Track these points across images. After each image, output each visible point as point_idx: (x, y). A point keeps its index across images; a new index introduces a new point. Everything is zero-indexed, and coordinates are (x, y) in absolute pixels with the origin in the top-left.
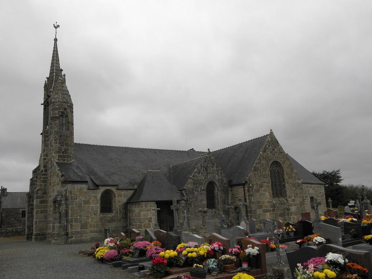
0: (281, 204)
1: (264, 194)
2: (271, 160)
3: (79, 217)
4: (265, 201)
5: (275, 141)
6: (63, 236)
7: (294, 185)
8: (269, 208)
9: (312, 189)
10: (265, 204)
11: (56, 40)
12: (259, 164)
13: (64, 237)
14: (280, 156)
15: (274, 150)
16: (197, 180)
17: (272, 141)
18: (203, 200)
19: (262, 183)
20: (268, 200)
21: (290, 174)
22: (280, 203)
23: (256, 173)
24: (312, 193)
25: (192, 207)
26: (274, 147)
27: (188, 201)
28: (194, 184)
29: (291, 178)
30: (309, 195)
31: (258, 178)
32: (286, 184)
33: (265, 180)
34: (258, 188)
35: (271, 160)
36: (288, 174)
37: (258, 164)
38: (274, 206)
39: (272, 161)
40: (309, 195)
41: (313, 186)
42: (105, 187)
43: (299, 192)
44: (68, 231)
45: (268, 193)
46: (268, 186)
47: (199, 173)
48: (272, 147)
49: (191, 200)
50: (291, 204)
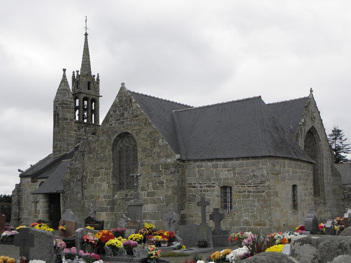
0: (125, 201)
1: (100, 186)
2: (116, 132)
3: (27, 206)
4: (100, 195)
5: (125, 100)
6: (13, 221)
7: (155, 168)
8: (106, 206)
9: (228, 171)
10: (100, 200)
11: (86, 35)
12: (97, 143)
13: (14, 221)
14: (132, 123)
15: (122, 115)
16: (74, 168)
17: (121, 101)
18: (79, 192)
19: (98, 169)
20: (105, 194)
21: (148, 149)
22: (124, 198)
23: (91, 156)
24: (227, 179)
25: (68, 200)
26: (124, 110)
27: (64, 194)
28: (71, 174)
29: (151, 156)
30: (217, 183)
31: (94, 162)
32: (140, 167)
33: (103, 164)
34: (93, 177)
35: (116, 132)
36: (144, 150)
37: (95, 142)
38: (113, 203)
39: (116, 135)
40: (217, 183)
41: (230, 163)
42: (41, 180)
43: (167, 180)
44: (20, 217)
45: (107, 183)
46: (107, 174)
47: (76, 161)
48: (119, 112)
49: (67, 193)
50: (145, 200)
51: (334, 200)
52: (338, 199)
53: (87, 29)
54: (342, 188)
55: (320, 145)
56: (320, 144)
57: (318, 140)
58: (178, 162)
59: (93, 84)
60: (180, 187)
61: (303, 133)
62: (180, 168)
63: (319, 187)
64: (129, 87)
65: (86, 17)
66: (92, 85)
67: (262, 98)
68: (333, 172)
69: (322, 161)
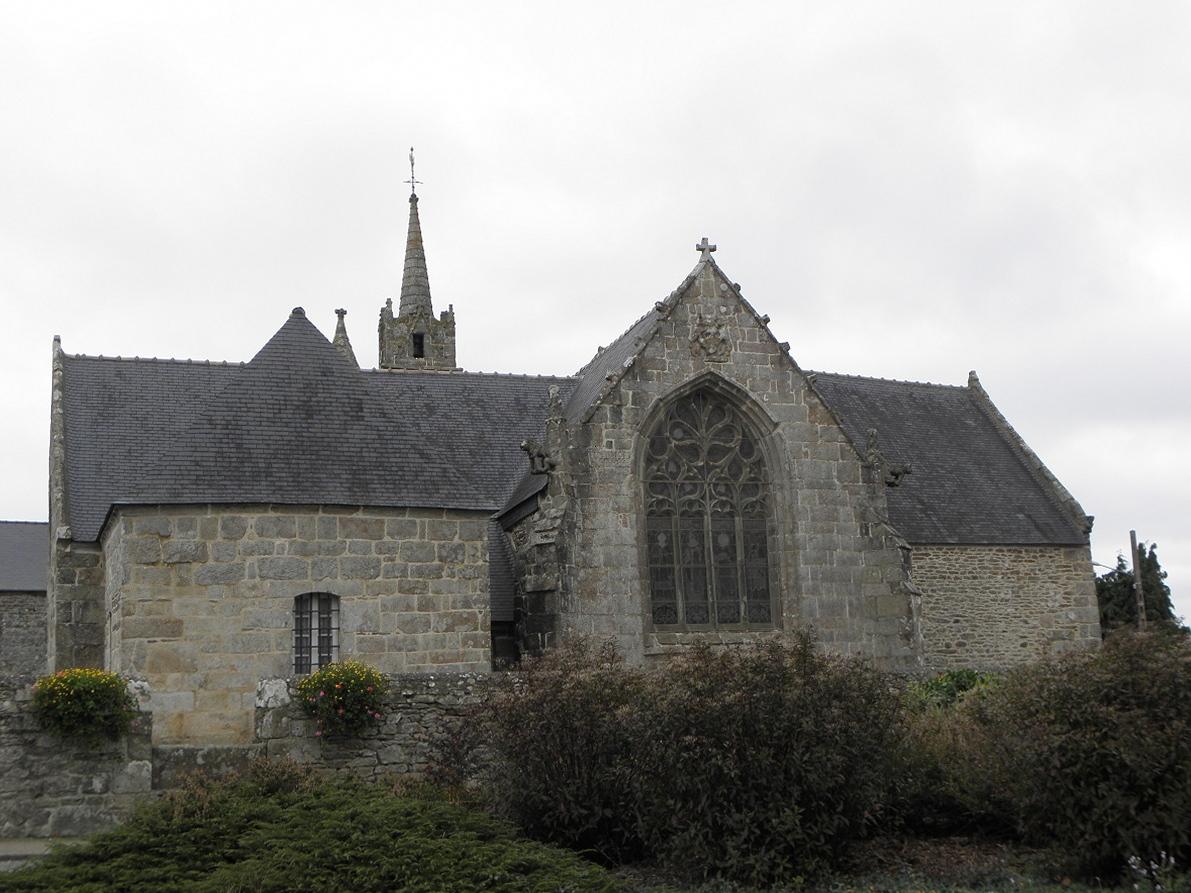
11: (414, 199)
51: (870, 640)
52: (886, 636)
53: (416, 185)
54: (901, 591)
55: (777, 439)
56: (779, 435)
57: (761, 420)
58: (68, 550)
59: (433, 338)
60: (73, 623)
61: (629, 405)
62: (79, 566)
63: (781, 596)
64: (70, 349)
65: (412, 150)
66: (428, 341)
67: (306, 316)
68: (867, 533)
69: (788, 498)
